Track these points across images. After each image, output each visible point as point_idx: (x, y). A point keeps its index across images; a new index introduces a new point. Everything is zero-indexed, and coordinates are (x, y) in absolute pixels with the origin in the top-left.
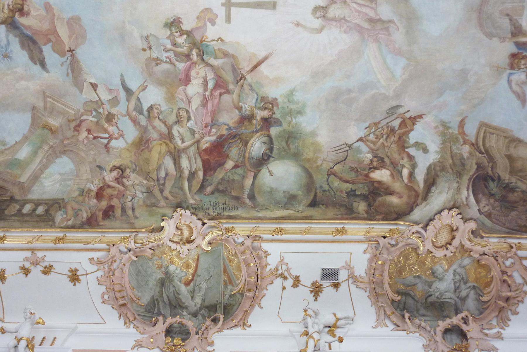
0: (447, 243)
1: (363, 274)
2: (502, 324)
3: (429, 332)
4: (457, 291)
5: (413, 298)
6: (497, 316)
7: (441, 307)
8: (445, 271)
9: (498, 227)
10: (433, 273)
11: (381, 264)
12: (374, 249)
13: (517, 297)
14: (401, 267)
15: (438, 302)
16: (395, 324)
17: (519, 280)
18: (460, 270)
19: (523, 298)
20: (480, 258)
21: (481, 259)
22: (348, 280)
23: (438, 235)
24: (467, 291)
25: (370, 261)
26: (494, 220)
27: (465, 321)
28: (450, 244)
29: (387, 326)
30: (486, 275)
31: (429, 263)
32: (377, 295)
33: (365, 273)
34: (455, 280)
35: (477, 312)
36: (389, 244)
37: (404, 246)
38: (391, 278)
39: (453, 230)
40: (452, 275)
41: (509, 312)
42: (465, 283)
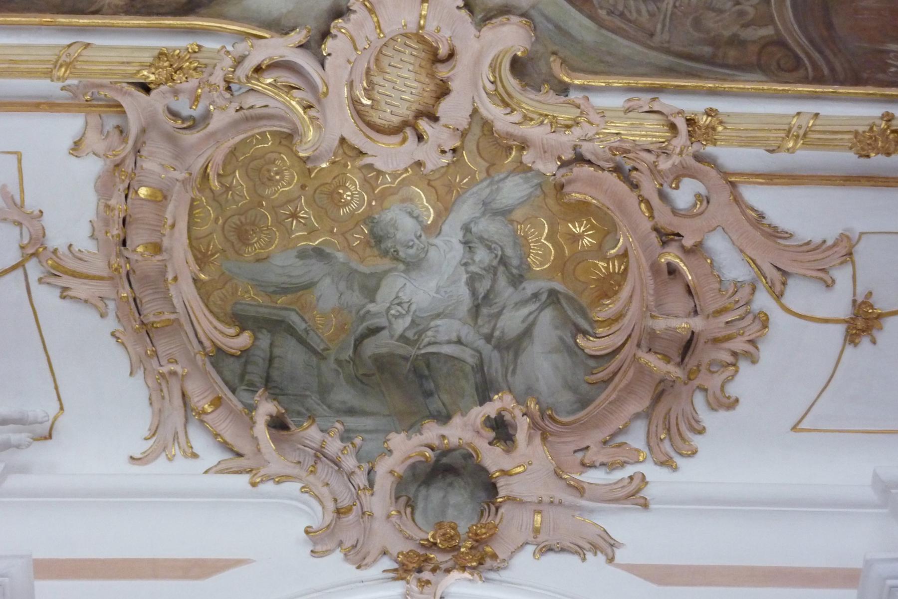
0: (419, 115)
1: (84, 243)
2: (667, 446)
3: (350, 475)
4: (485, 311)
5: (302, 341)
6: (647, 414)
7: (421, 377)
8: (426, 229)
9: (624, 46)
10: (378, 239)
11: (151, 200)
12: (115, 137)
13: (728, 338)
14: (242, 212)
15: (405, 359)
16: (226, 446)
17: (734, 269)
18: (489, 227)
19: (751, 342)
20: (563, 175)
21: (570, 182)
22: (20, 265)
23: (377, 79)
24: (524, 311)
25: (104, 186)
26: (602, 13)
27: (501, 430)
28: (434, 118)
29: (195, 456)
30: (600, 246)
31: (353, 193)
32: (148, 330)
33: (92, 237)
34: (473, 268)
35: (566, 398)
36: (174, 114)
37: (234, 125)
38: (202, 259)
39: (438, 58)
40: (459, 250)
41: (699, 400)
42: (516, 280)
